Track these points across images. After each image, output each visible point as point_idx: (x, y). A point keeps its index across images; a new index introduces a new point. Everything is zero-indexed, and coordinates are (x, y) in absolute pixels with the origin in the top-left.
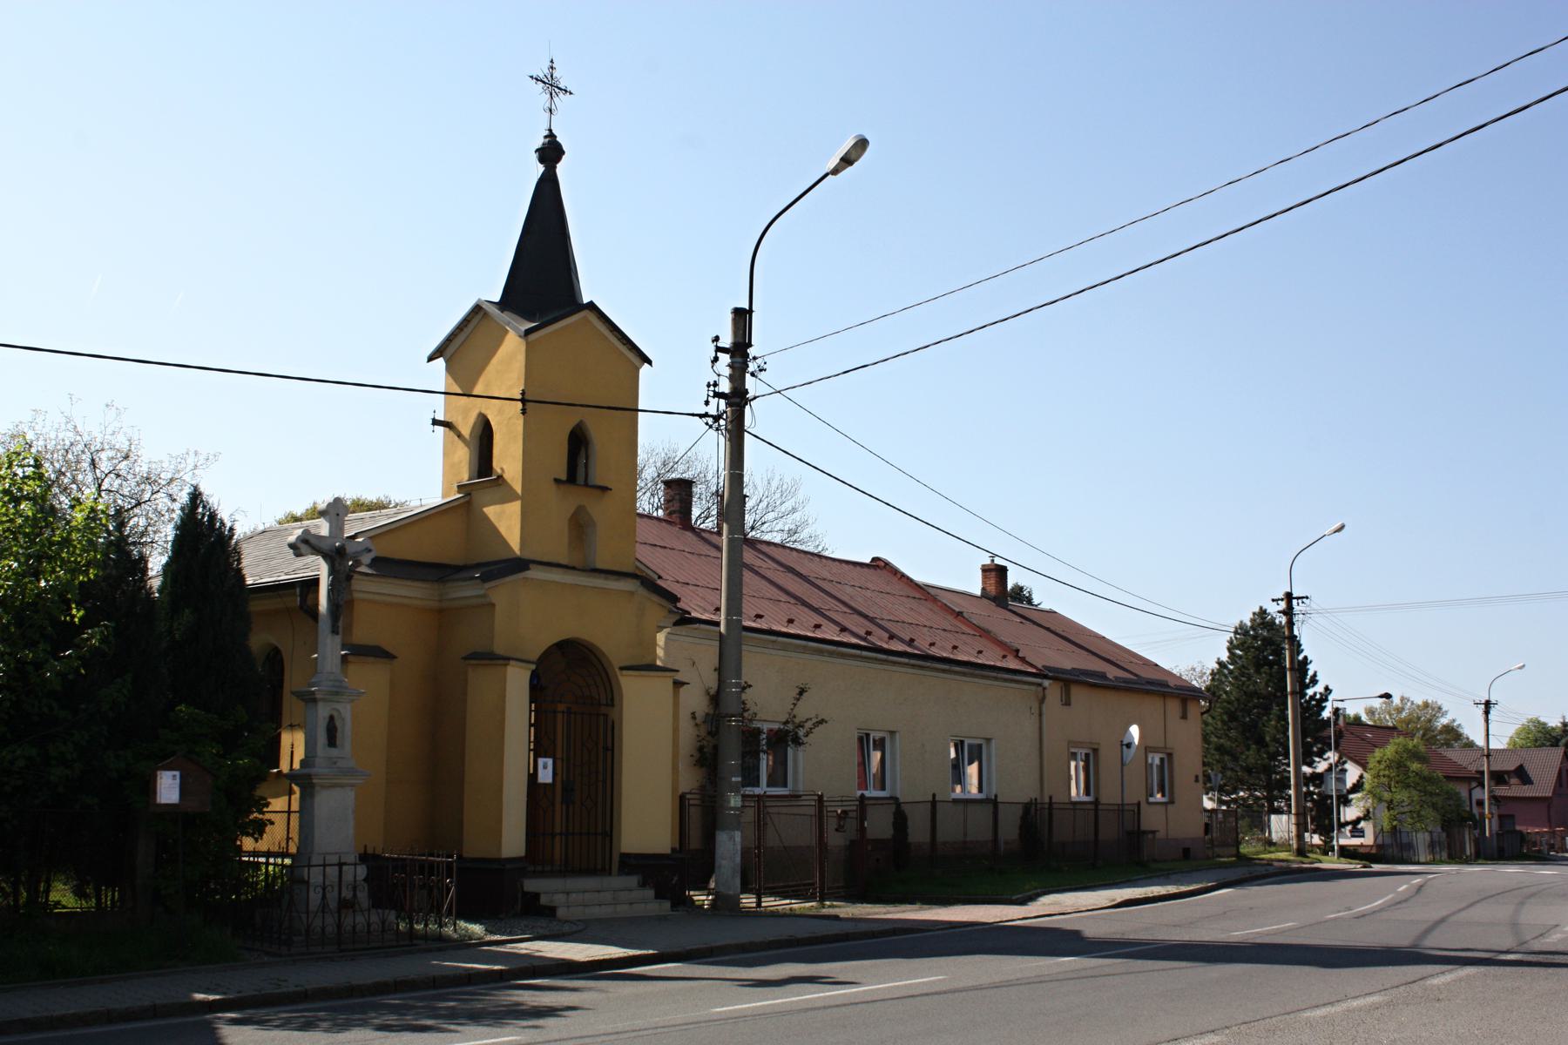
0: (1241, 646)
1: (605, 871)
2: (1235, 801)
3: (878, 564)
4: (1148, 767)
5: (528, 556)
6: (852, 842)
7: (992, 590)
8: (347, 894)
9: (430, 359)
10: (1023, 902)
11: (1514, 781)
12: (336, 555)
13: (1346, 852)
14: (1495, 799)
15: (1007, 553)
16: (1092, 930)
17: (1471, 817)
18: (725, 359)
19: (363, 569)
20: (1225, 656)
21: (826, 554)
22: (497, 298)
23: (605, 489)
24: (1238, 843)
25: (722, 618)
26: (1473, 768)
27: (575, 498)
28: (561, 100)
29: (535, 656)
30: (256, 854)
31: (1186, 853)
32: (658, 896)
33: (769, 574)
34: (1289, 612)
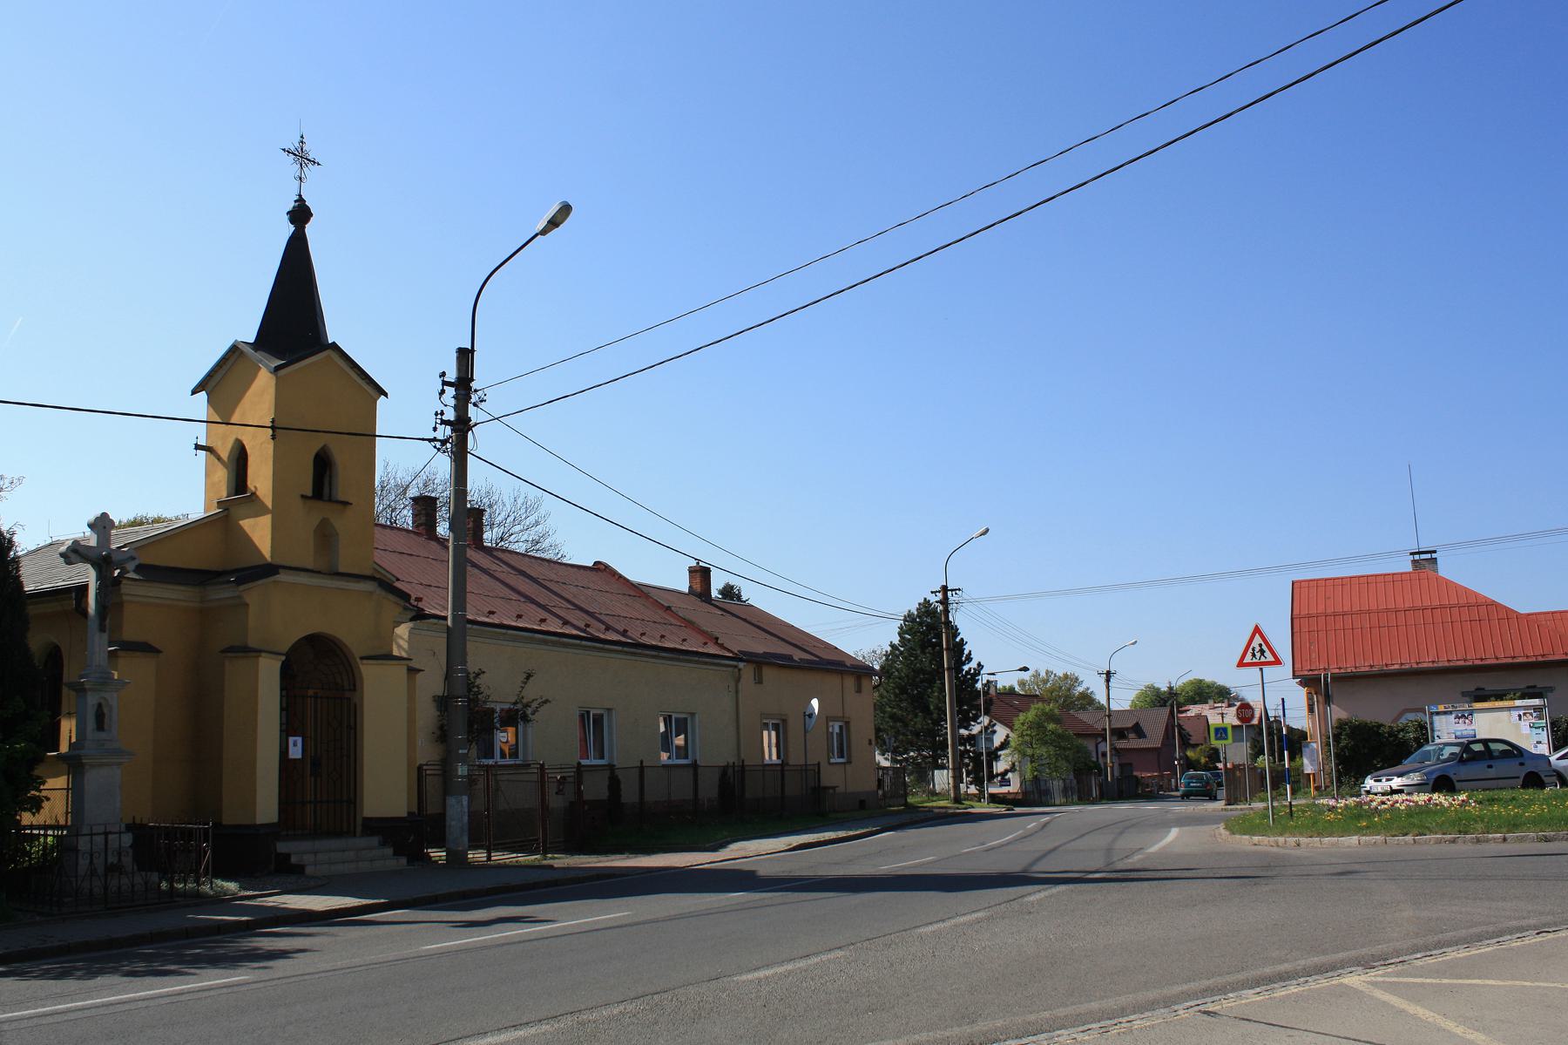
2: (906, 760)
3: (600, 568)
4: (830, 735)
5: (278, 562)
6: (571, 803)
7: (698, 588)
8: (112, 859)
9: (194, 392)
10: (714, 849)
11: (1132, 735)
12: (102, 561)
13: (994, 799)
14: (1116, 752)
15: (708, 557)
16: (764, 870)
17: (1097, 765)
18: (450, 391)
19: (131, 575)
20: (896, 640)
21: (565, 561)
22: (252, 340)
23: (346, 503)
24: (906, 795)
25: (449, 614)
26: (1099, 727)
27: (322, 510)
28: (310, 171)
29: (285, 648)
30: (32, 827)
31: (862, 804)
32: (395, 854)
33: (501, 576)
34: (945, 602)
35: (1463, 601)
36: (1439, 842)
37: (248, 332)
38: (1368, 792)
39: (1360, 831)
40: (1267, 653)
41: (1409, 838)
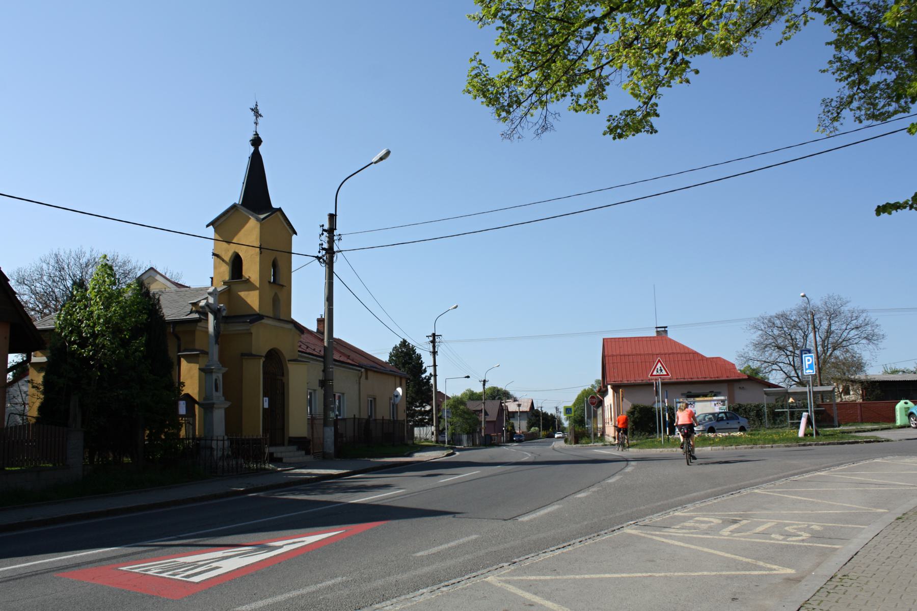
0: (396, 355)
5: (261, 313)
9: (208, 226)
23: (283, 286)
29: (264, 354)
37: (236, 197)
39: (710, 445)
41: (733, 447)
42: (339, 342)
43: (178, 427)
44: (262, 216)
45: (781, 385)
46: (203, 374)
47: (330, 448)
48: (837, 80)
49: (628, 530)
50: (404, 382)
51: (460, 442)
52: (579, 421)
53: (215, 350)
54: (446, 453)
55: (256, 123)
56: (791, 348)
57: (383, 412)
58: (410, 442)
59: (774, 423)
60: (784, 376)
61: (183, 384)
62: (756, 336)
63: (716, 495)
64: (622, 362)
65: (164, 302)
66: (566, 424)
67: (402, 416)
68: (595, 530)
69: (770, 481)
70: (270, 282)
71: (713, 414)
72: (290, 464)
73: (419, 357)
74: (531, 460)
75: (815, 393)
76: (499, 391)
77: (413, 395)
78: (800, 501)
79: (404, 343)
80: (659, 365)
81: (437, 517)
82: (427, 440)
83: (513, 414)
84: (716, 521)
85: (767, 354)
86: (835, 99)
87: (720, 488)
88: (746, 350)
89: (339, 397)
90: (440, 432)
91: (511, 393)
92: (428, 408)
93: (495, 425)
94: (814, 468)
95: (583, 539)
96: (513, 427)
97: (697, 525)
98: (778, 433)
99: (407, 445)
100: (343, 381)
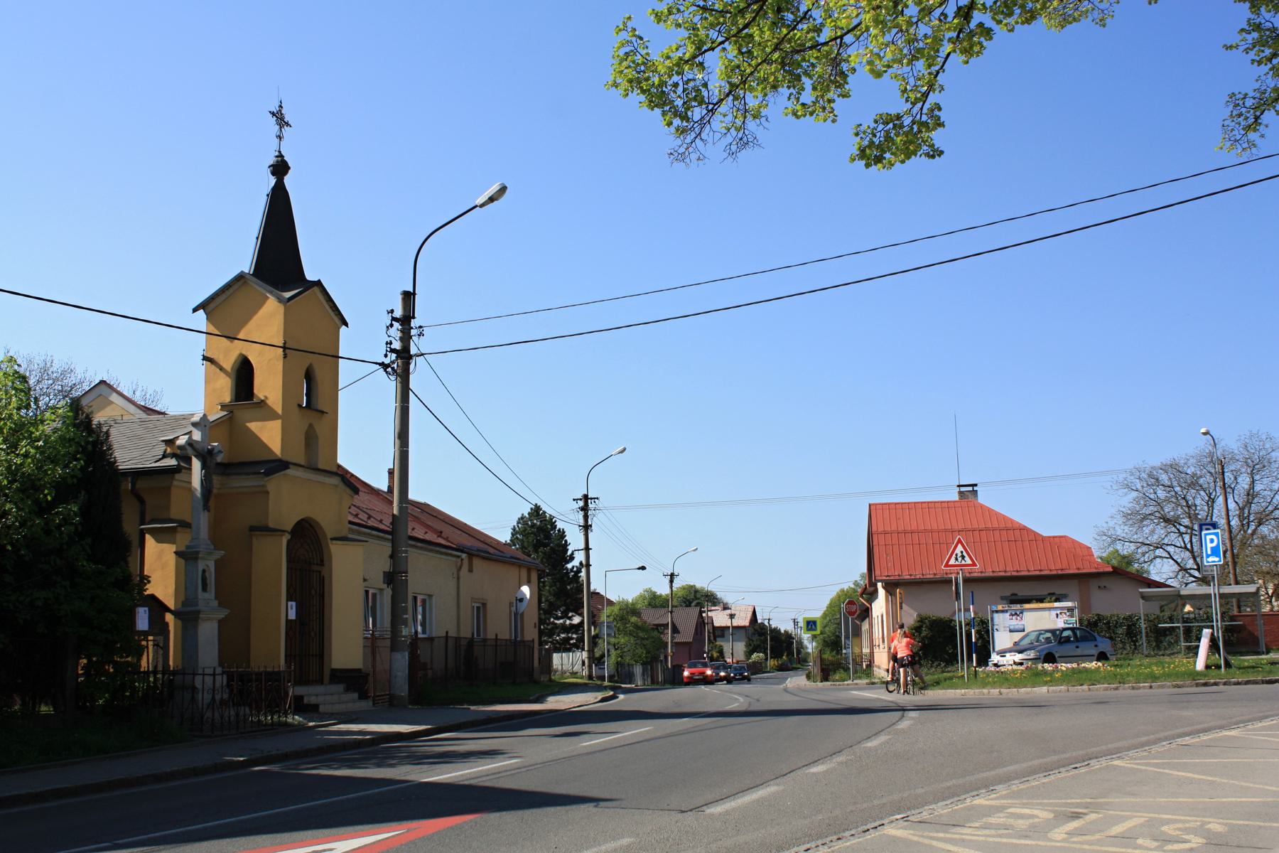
0: (523, 532)
1: (320, 681)
5: (286, 458)
9: (195, 310)
23: (323, 412)
29: (289, 528)
35: (1003, 526)
36: (1106, 689)
37: (244, 261)
38: (996, 665)
39: (1046, 683)
40: (967, 558)
41: (1085, 687)
42: (425, 508)
43: (139, 652)
44: (288, 295)
45: (1169, 582)
46: (182, 561)
47: (402, 687)
48: (1253, 61)
49: (890, 831)
50: (534, 576)
51: (630, 678)
52: (833, 644)
53: (203, 522)
54: (600, 695)
55: (280, 137)
56: (1186, 522)
57: (498, 627)
58: (544, 678)
59: (1158, 647)
60: (1176, 568)
61: (145, 579)
62: (1127, 500)
63: (1047, 769)
64: (901, 547)
65: (116, 437)
66: (810, 646)
67: (531, 634)
68: (835, 829)
69: (1143, 745)
70: (300, 406)
71: (1053, 632)
72: (331, 716)
73: (562, 534)
74: (743, 708)
75: (1222, 596)
76: (696, 591)
77: (551, 598)
78: (1191, 781)
79: (536, 511)
80: (960, 548)
81: (568, 808)
82: (574, 674)
83: (721, 632)
84: (1044, 815)
85: (1146, 530)
86: (1251, 94)
87: (1055, 758)
88: (1111, 524)
89: (424, 601)
90: (596, 660)
91: (719, 595)
92: (576, 620)
93: (692, 651)
94: (1219, 723)
95: (813, 845)
96: (721, 652)
97: (1011, 821)
98: (1161, 664)
99: (536, 682)
100: (426, 574)
